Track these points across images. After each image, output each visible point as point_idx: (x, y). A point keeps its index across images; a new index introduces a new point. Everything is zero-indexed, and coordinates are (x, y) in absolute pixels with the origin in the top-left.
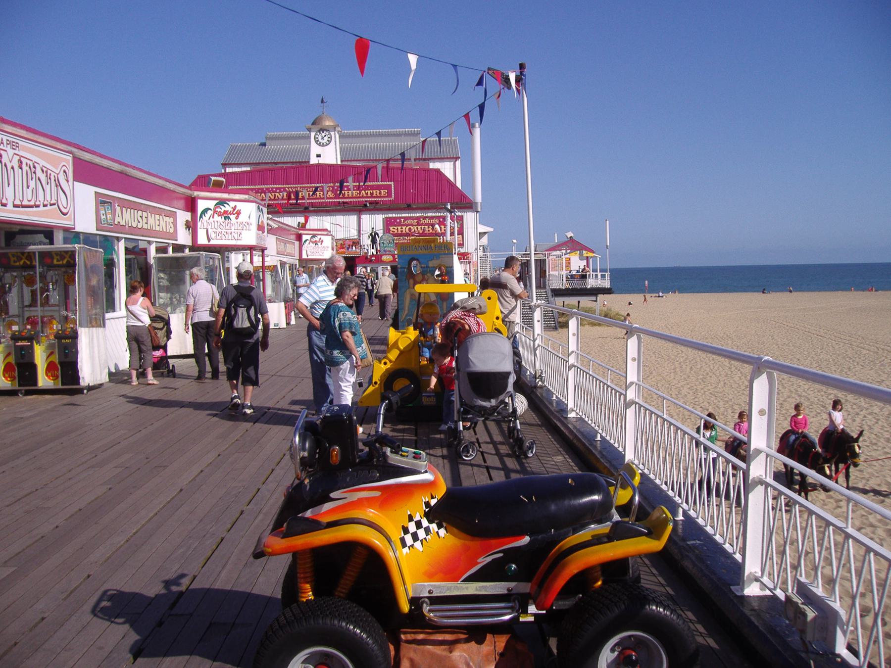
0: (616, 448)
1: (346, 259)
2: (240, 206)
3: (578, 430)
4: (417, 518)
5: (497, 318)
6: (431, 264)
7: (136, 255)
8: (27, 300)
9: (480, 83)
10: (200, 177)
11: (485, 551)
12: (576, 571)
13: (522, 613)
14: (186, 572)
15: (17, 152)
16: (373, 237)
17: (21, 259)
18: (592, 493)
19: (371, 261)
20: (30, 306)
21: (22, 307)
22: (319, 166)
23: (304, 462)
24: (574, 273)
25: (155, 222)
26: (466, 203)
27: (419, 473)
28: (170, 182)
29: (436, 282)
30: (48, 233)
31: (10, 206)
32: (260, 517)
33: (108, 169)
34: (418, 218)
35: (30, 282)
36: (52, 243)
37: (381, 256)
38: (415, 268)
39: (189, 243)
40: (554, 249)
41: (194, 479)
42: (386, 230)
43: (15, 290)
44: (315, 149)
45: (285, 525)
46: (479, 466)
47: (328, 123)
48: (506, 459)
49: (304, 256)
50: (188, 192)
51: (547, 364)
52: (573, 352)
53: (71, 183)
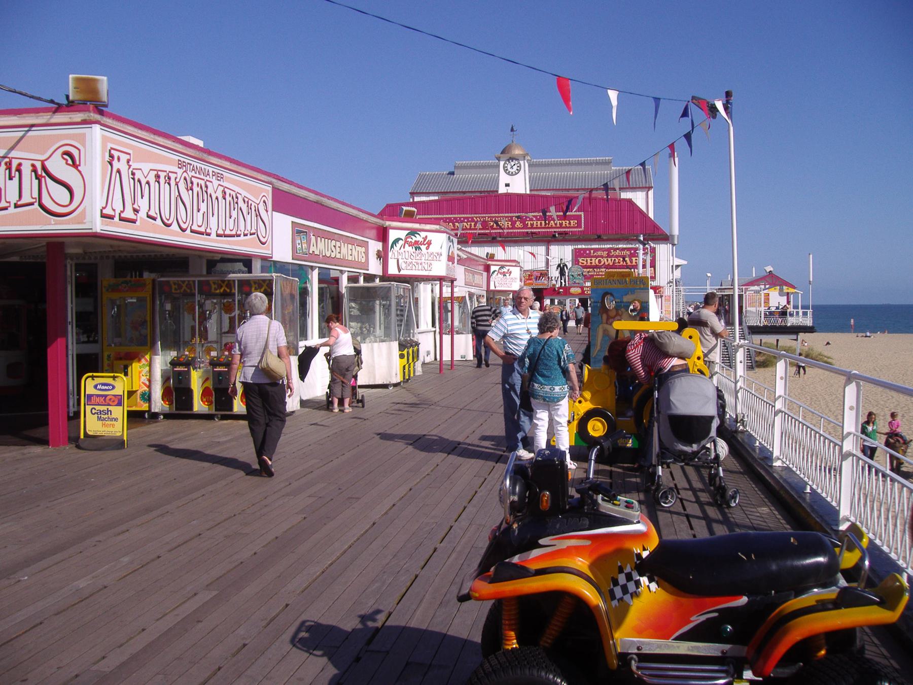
0: (829, 503)
1: (534, 290)
2: (431, 236)
3: (785, 480)
4: (628, 569)
5: (699, 358)
6: (625, 299)
7: (329, 283)
8: (226, 326)
9: (685, 114)
10: (388, 206)
11: (698, 610)
12: (799, 638)
13: (738, 678)
14: (381, 608)
15: (221, 183)
16: (562, 268)
17: (221, 287)
18: (817, 554)
19: (559, 293)
20: (228, 332)
21: (221, 334)
22: (507, 195)
23: (514, 508)
24: (773, 309)
25: (347, 252)
26: (665, 238)
27: (631, 523)
28: (354, 208)
29: (633, 318)
30: (247, 261)
31: (214, 235)
32: (454, 555)
33: (305, 199)
34: (609, 250)
35: (228, 309)
36: (250, 271)
37: (570, 288)
38: (610, 304)
39: (379, 272)
40: (752, 283)
41: (386, 513)
42: (575, 261)
43: (214, 317)
44: (504, 178)
45: (492, 569)
46: (678, 514)
47: (517, 152)
48: (706, 507)
49: (492, 288)
50: (379, 221)
51: (751, 408)
52: (780, 397)
53: (270, 213)
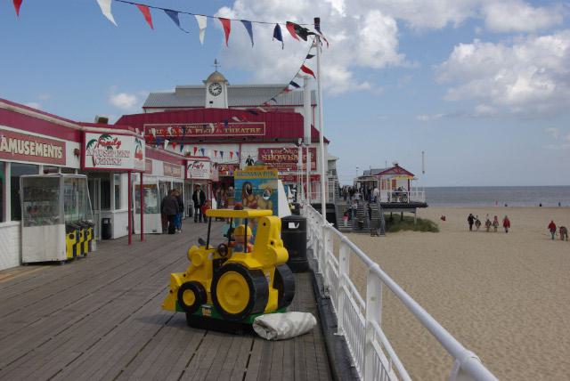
10: (123, 116)
16: (249, 162)
22: (212, 110)
42: (260, 157)
44: (209, 97)
49: (189, 177)
